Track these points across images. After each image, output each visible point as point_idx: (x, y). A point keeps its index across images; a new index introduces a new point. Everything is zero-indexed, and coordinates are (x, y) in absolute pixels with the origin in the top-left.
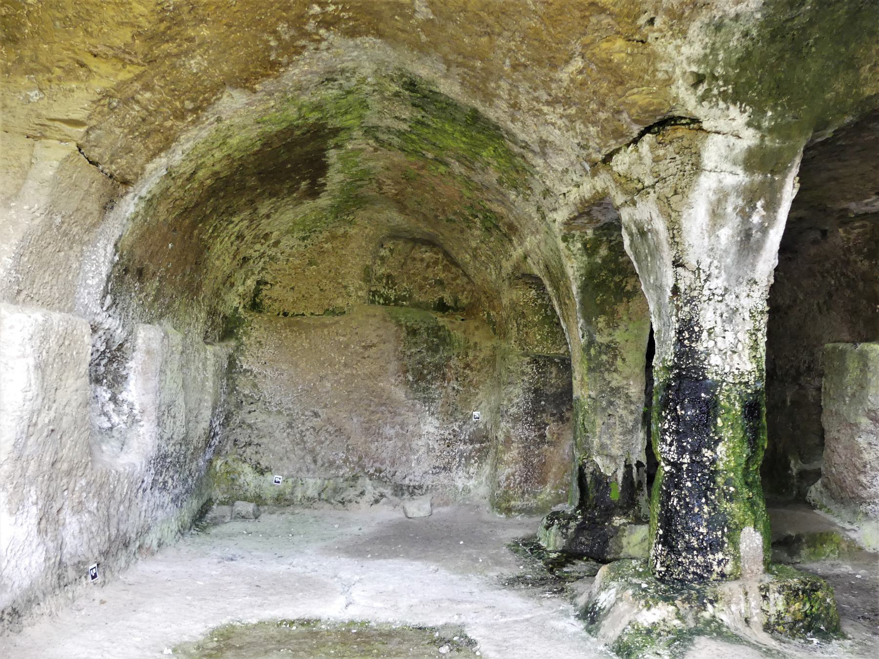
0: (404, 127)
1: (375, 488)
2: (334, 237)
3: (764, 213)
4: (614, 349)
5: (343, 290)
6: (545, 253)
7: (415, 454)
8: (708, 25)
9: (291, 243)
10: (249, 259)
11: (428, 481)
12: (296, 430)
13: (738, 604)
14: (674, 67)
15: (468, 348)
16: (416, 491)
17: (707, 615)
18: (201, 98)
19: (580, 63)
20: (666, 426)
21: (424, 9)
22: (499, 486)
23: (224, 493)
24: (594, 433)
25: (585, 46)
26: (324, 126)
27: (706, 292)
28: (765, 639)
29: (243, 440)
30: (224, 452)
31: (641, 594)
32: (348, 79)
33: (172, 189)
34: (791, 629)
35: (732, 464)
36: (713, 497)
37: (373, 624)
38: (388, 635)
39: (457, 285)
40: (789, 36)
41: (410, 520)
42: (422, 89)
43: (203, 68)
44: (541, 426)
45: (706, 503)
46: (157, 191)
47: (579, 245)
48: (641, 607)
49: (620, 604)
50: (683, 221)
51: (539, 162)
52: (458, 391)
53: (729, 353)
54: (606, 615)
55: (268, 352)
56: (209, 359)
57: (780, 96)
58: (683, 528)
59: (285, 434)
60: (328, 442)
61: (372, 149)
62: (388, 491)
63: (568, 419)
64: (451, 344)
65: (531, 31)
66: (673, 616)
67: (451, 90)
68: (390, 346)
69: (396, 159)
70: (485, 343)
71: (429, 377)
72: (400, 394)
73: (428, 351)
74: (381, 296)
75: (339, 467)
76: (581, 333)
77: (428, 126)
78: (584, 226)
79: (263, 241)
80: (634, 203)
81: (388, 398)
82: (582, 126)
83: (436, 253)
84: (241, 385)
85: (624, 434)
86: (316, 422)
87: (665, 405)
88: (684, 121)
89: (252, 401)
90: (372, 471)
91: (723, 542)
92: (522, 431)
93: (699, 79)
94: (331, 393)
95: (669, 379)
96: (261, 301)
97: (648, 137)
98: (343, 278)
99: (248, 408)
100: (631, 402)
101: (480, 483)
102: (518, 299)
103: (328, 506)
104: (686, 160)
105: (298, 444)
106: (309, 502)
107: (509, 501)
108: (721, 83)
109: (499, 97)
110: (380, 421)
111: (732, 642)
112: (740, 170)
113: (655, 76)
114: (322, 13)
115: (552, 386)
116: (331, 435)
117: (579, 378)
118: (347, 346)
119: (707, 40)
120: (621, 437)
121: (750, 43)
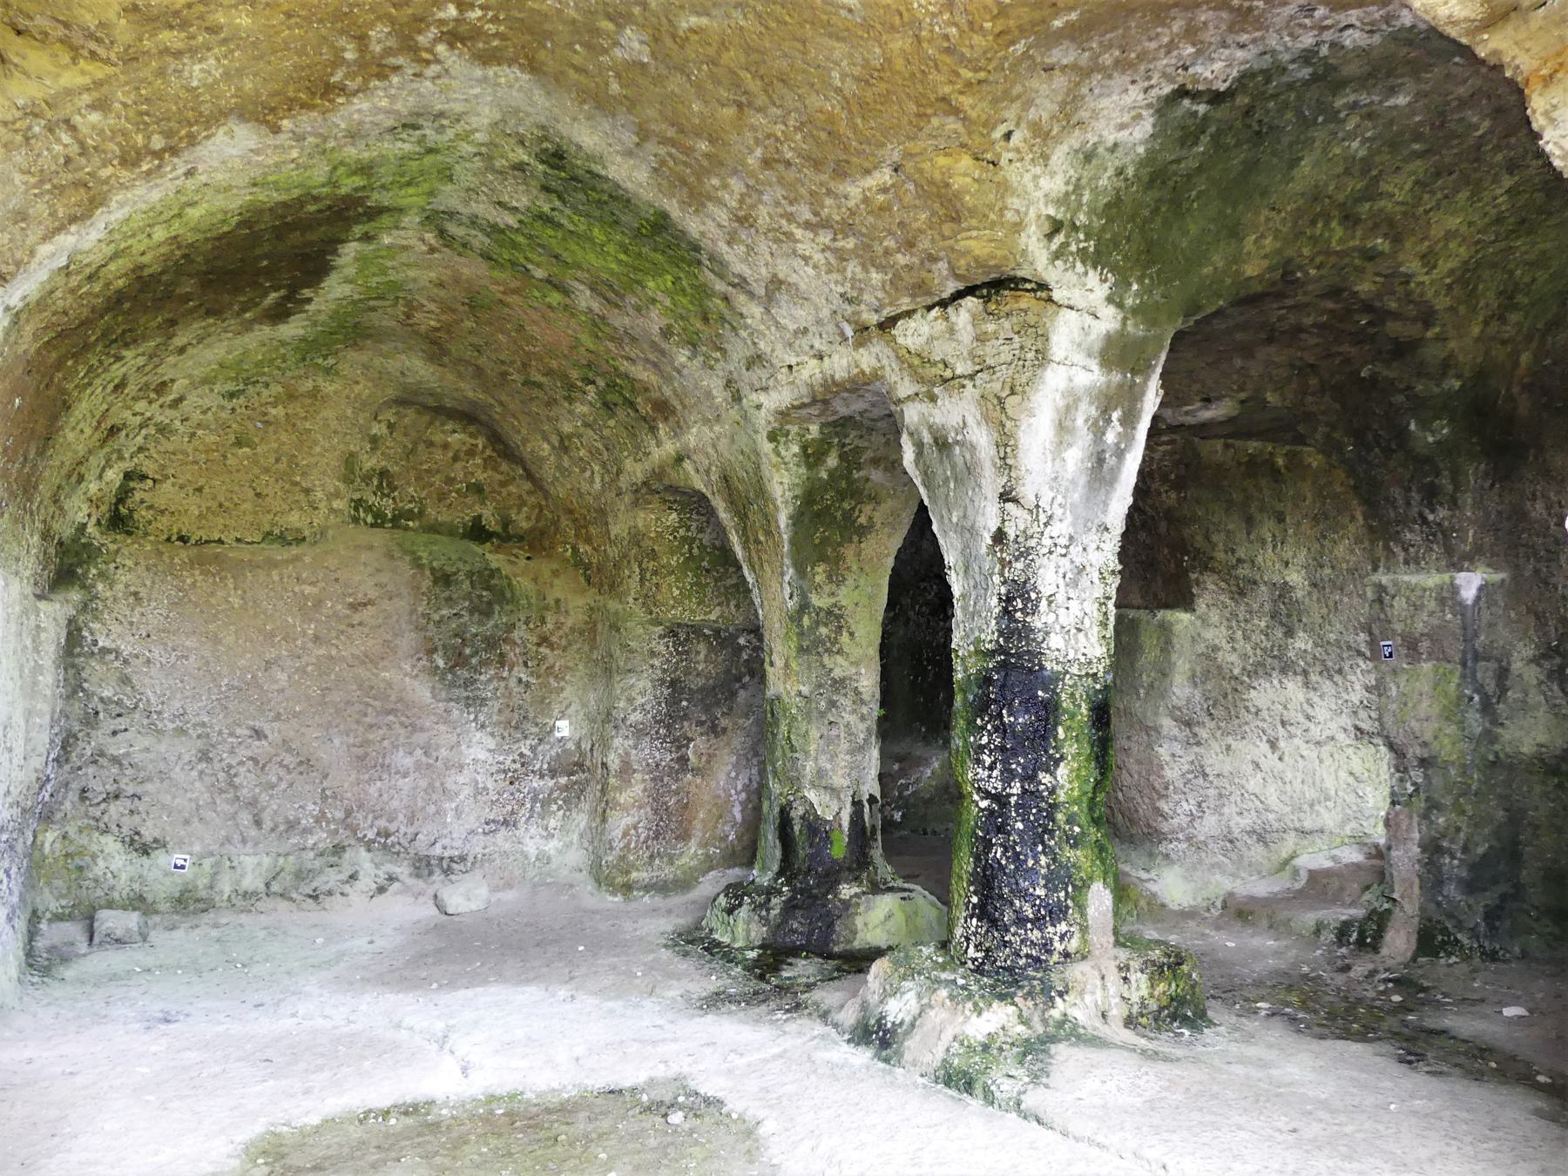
0: (511, 220)
1: (377, 866)
2: (291, 396)
3: (1120, 429)
4: (839, 617)
5: (301, 497)
6: (726, 454)
7: (452, 800)
8: (1076, 151)
9: (207, 402)
10: (119, 430)
11: (477, 847)
12: (217, 766)
13: (1093, 993)
14: (1028, 207)
15: (547, 608)
16: (455, 866)
17: (1055, 1014)
18: (183, 132)
19: (887, 177)
20: (985, 740)
21: (636, 45)
22: (611, 848)
23: (62, 896)
24: (806, 753)
25: (908, 155)
26: (360, 201)
27: (1047, 542)
28: (1128, 1036)
29: (99, 788)
30: (59, 816)
31: (961, 995)
32: (441, 130)
33: (59, 294)
34: (1156, 1020)
35: (1076, 793)
36: (1052, 843)
37: (529, 1095)
38: (566, 1110)
39: (509, 494)
40: (1171, 183)
41: (456, 919)
42: (574, 166)
43: (210, 80)
44: (681, 743)
45: (1044, 852)
46: (34, 297)
47: (796, 449)
48: (967, 1013)
49: (932, 1013)
50: (1021, 434)
51: (754, 311)
52: (528, 685)
53: (1073, 631)
54: (907, 1033)
55: (155, 614)
56: (45, 630)
57: (1153, 262)
58: (1011, 891)
59: (194, 773)
60: (283, 785)
61: (424, 248)
62: (402, 870)
63: (724, 730)
64: (513, 600)
65: (822, 117)
66: (1015, 1020)
67: (630, 178)
68: (402, 604)
69: (466, 271)
70: (576, 603)
71: (474, 661)
72: (421, 691)
73: (471, 613)
74: (369, 509)
75: (307, 831)
76: (787, 590)
77: (560, 226)
78: (809, 419)
79: (153, 395)
80: (933, 399)
81: (400, 700)
82: (858, 269)
83: (472, 435)
84: (94, 679)
85: (851, 752)
86: (259, 748)
87: (982, 707)
88: (1028, 286)
89: (118, 710)
90: (371, 835)
91: (1067, 907)
92: (650, 753)
93: (1056, 227)
94: (289, 692)
95: (987, 670)
96: (131, 511)
97: (970, 302)
98: (304, 474)
99: (109, 724)
100: (863, 702)
101: (568, 846)
102: (647, 526)
103: (283, 905)
104: (1028, 343)
105: (221, 791)
106: (247, 899)
107: (628, 872)
108: (1082, 236)
109: (720, 202)
110: (386, 743)
111: (1094, 1046)
112: (1094, 365)
113: (1002, 216)
114: (456, 20)
115: (698, 675)
116: (289, 771)
117: (779, 663)
118: (319, 603)
119: (1072, 172)
120: (848, 757)
121: (1122, 185)
